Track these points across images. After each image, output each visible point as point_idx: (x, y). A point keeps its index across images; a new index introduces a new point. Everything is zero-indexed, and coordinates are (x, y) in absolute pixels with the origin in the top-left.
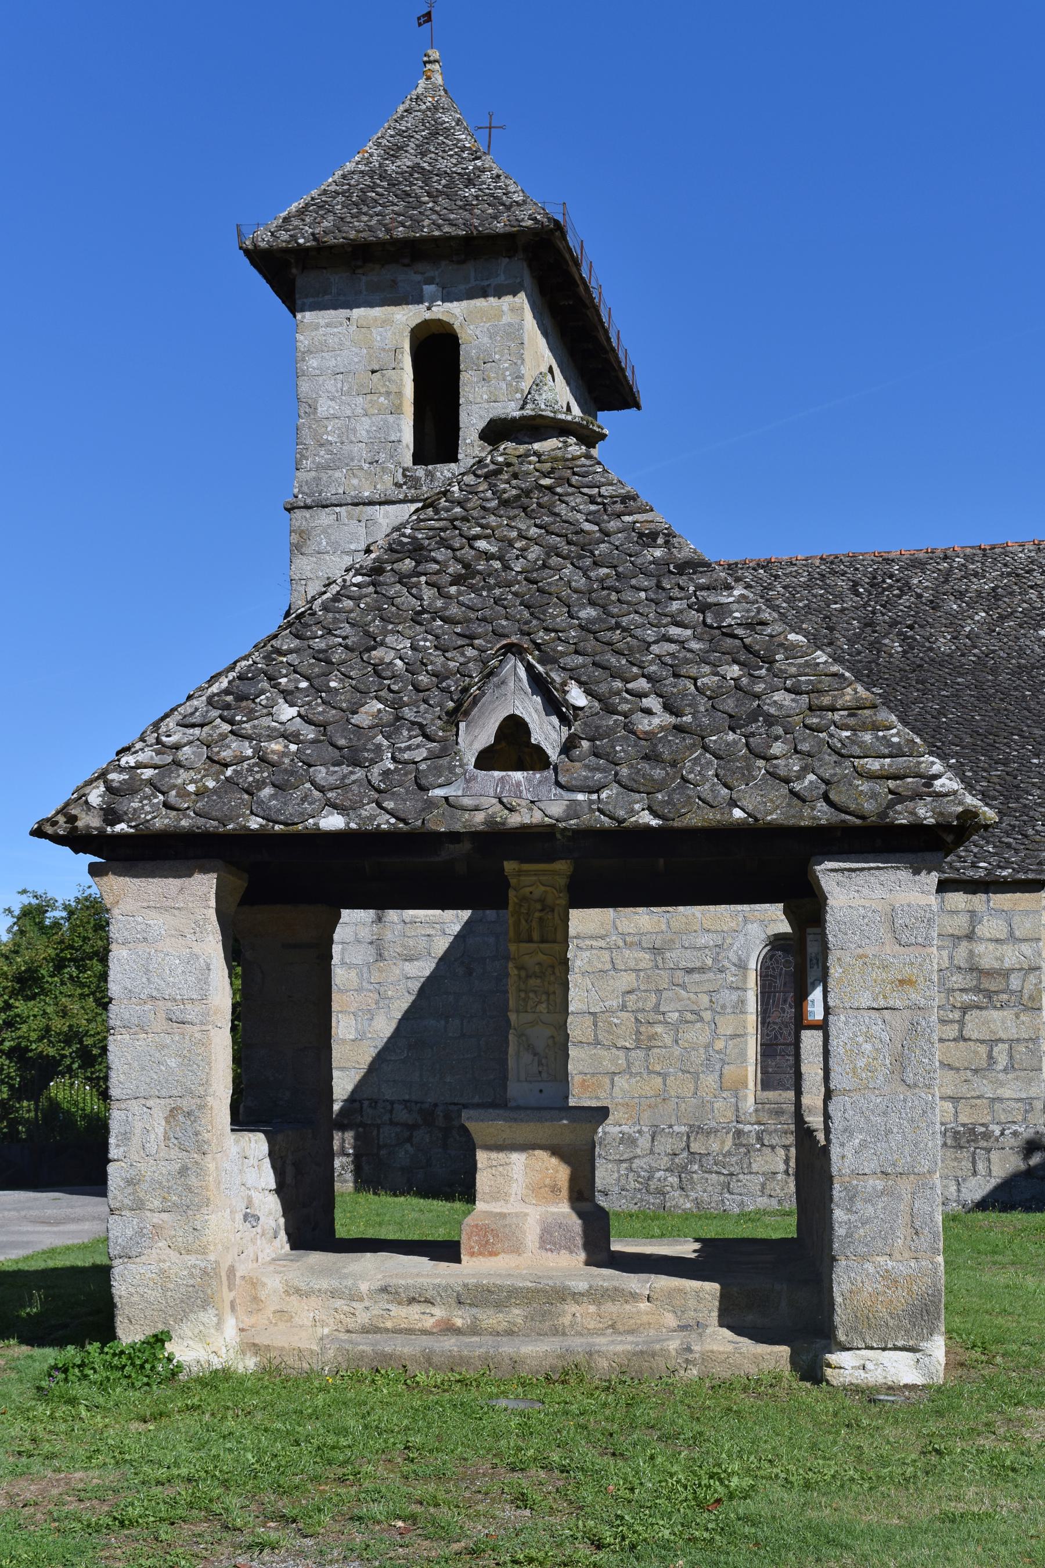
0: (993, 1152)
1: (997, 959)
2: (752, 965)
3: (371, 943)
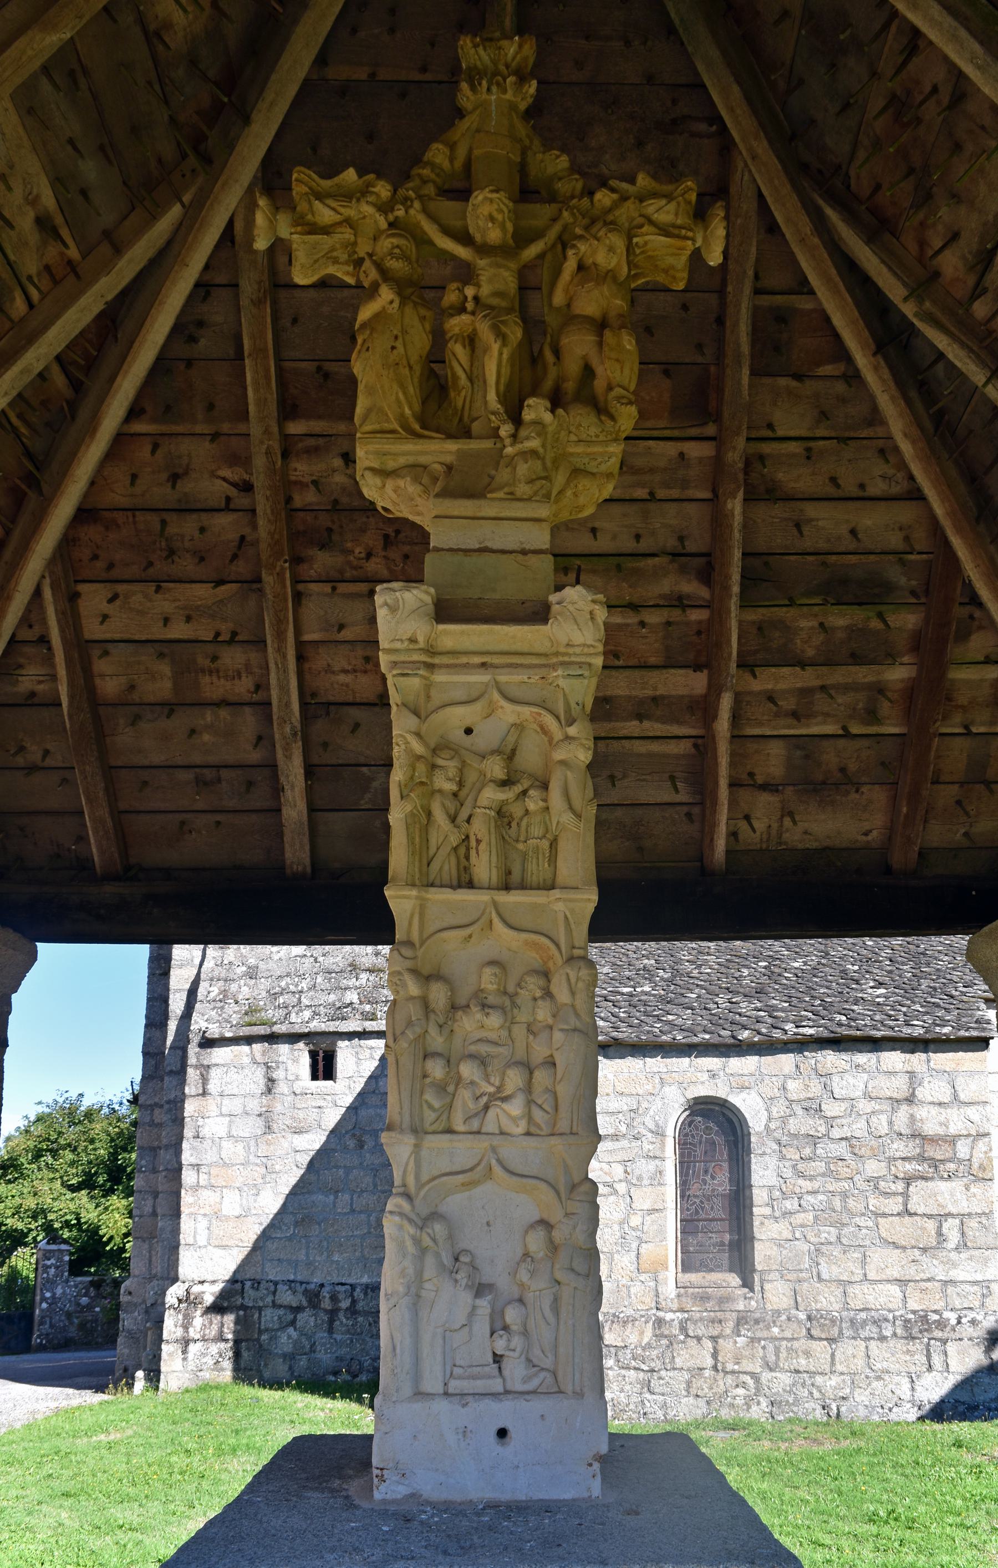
0: (949, 1344)
1: (941, 1124)
2: (670, 1131)
3: (260, 1115)
